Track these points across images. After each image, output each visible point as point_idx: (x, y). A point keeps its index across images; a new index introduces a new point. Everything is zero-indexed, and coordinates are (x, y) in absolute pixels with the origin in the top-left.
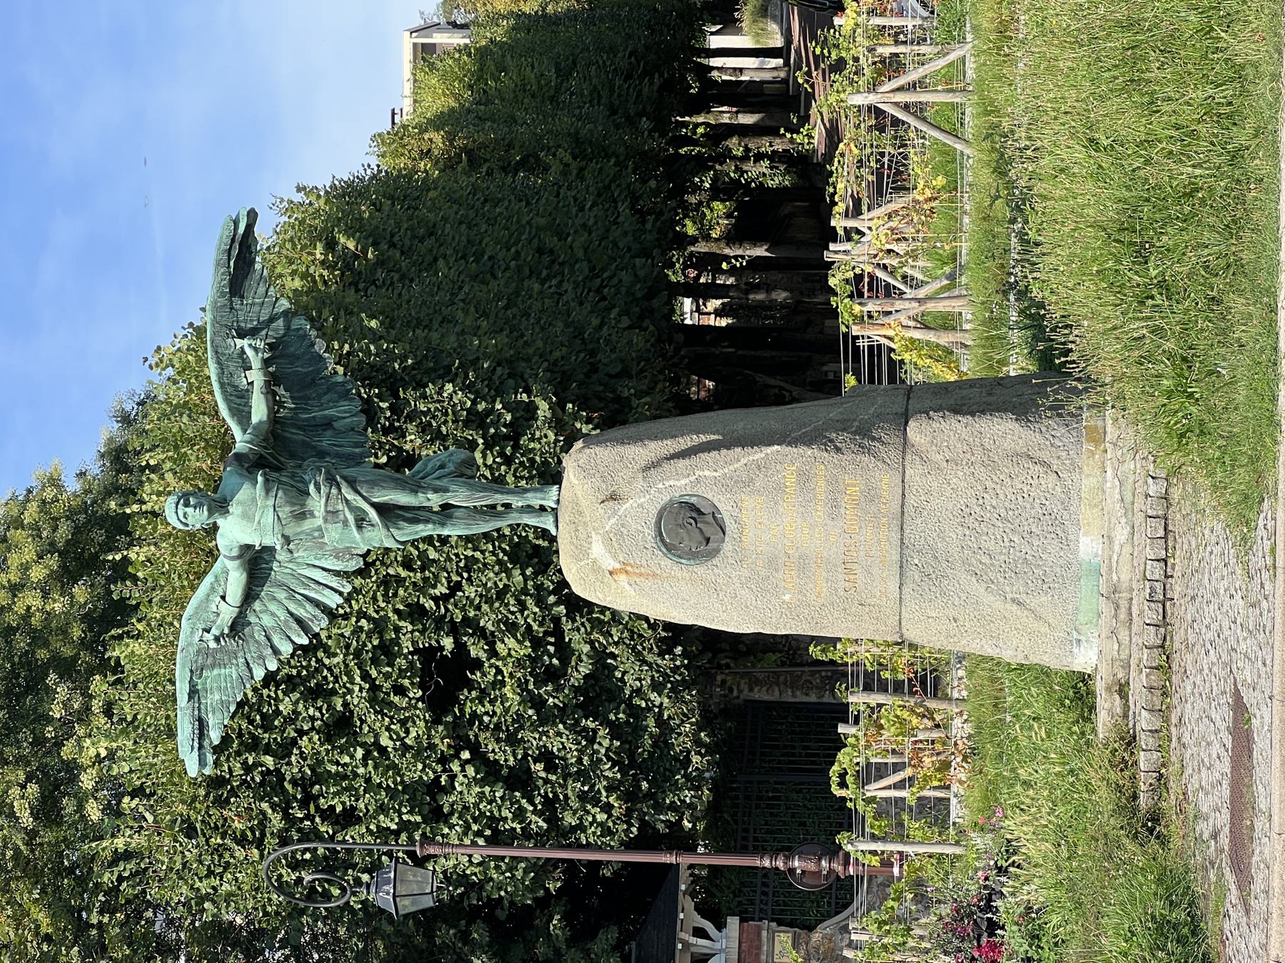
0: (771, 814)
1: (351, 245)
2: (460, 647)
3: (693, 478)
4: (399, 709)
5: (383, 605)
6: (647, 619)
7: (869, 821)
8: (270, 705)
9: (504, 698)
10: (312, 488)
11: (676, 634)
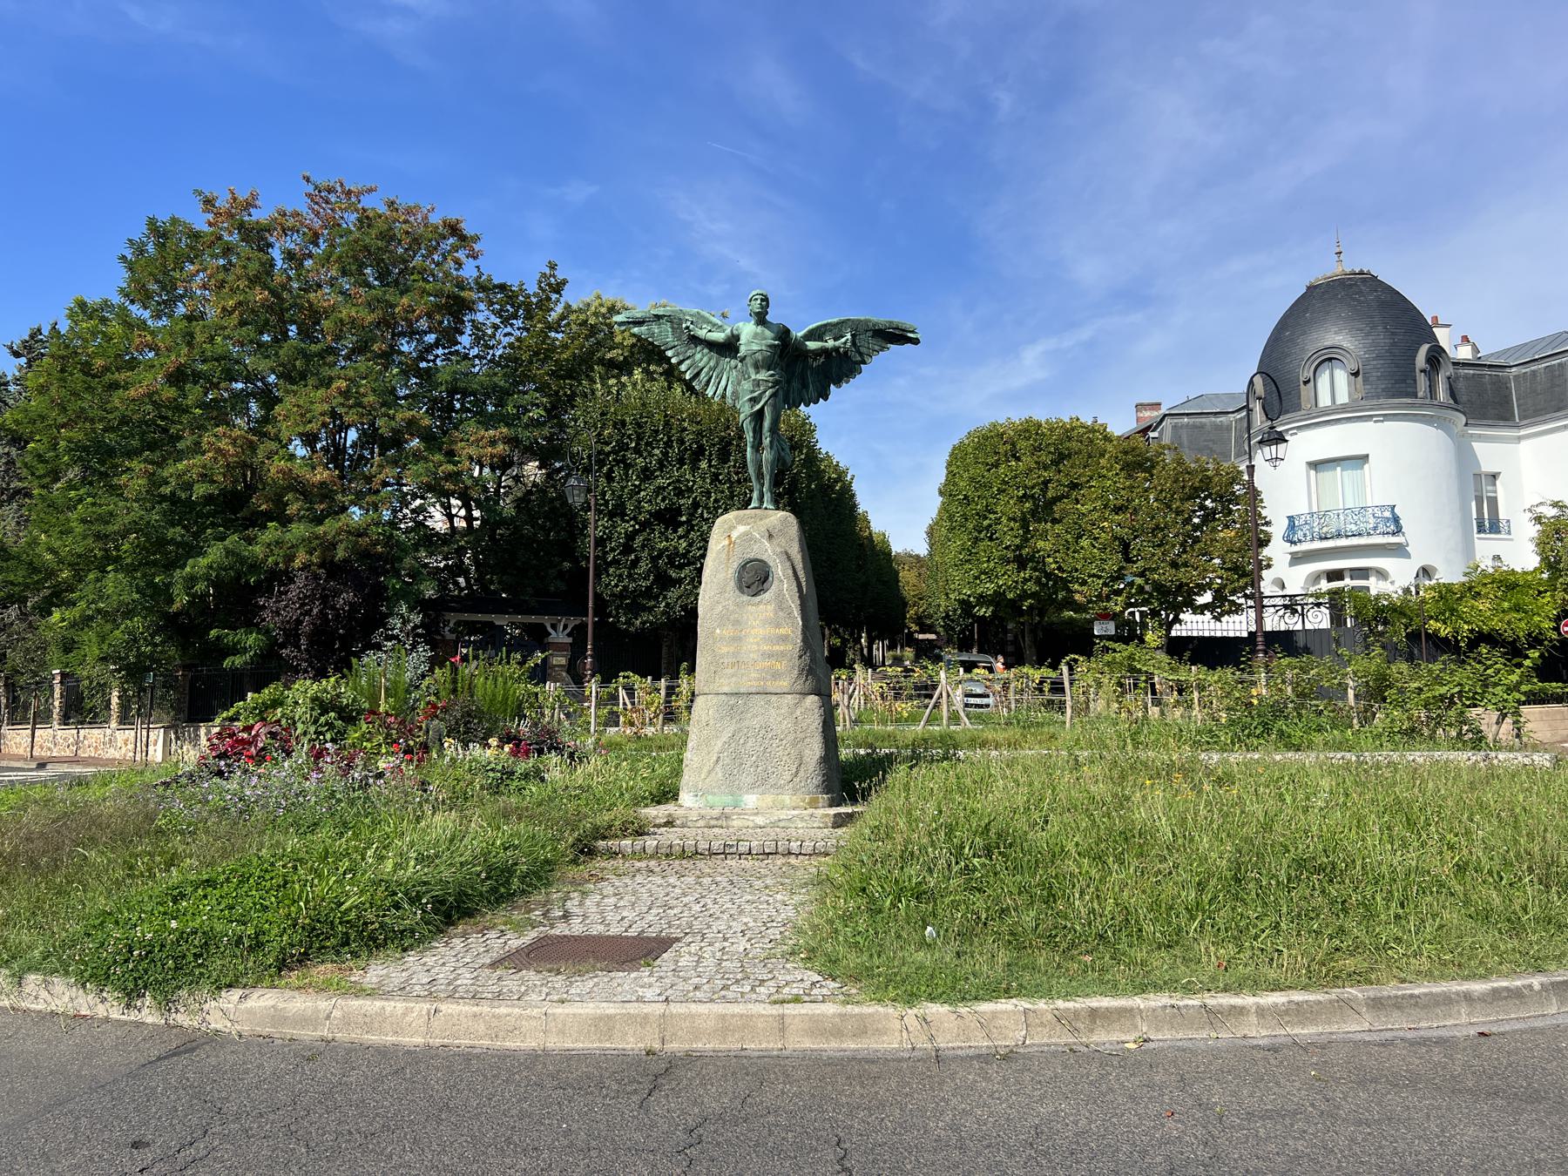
11: (693, 613)
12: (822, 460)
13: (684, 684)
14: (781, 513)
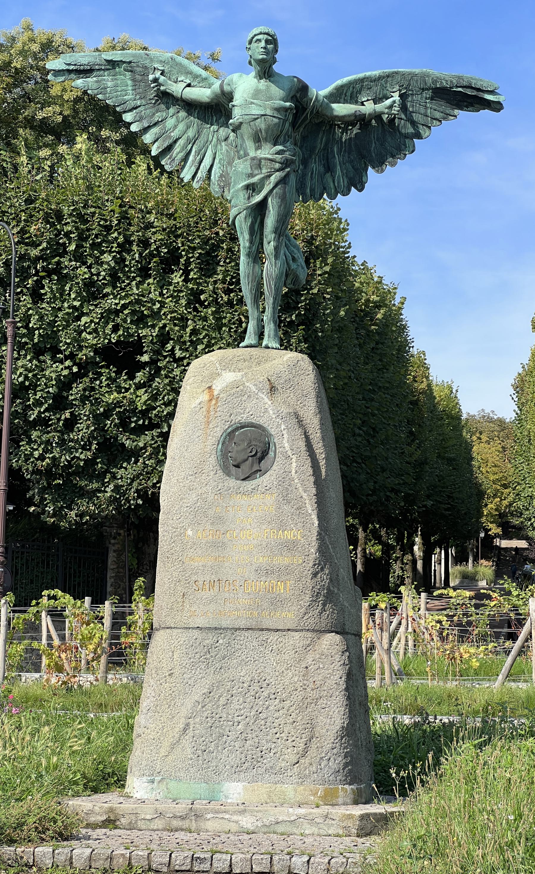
0: (38, 563)
1: (379, 316)
2: (142, 366)
3: (290, 453)
4: (104, 328)
5: (169, 317)
6: (159, 481)
7: (22, 616)
8: (107, 247)
9: (110, 393)
10: (280, 148)
11: (152, 502)
12: (357, 274)
13: (139, 603)
14: (290, 356)
